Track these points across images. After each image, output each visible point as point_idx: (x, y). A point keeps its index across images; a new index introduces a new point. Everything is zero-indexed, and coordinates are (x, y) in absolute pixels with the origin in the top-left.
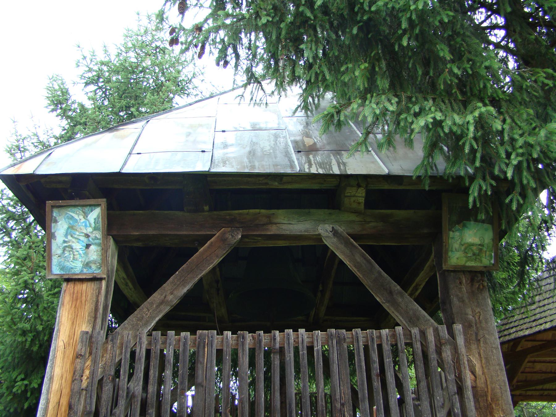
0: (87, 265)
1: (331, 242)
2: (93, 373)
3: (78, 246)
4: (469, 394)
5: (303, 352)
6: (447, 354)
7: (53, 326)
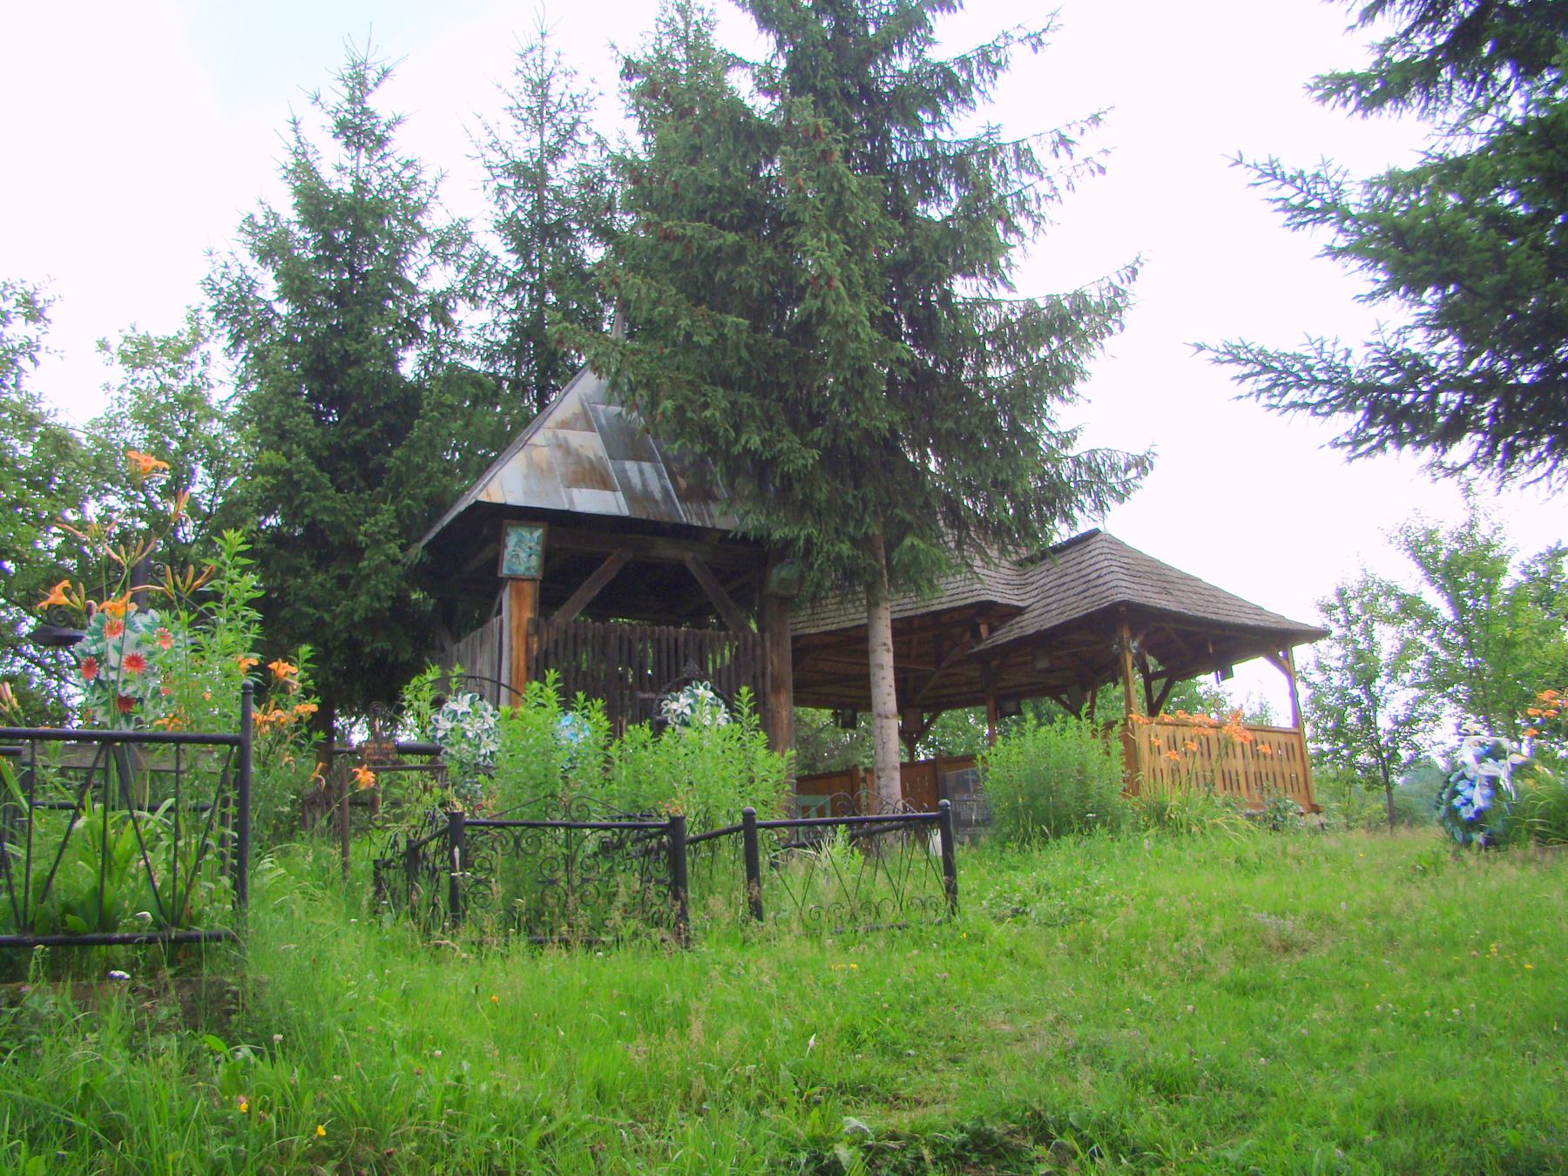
0: (528, 569)
1: (692, 568)
2: (540, 647)
3: (523, 555)
4: (768, 678)
5: (672, 642)
6: (759, 651)
7: (760, 704)
